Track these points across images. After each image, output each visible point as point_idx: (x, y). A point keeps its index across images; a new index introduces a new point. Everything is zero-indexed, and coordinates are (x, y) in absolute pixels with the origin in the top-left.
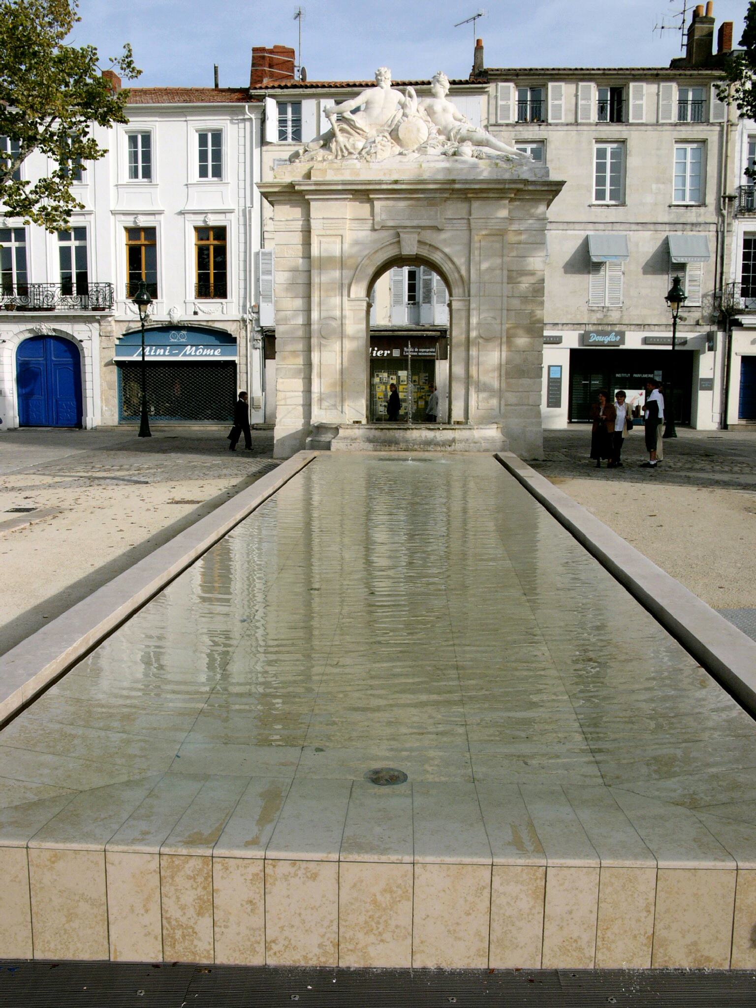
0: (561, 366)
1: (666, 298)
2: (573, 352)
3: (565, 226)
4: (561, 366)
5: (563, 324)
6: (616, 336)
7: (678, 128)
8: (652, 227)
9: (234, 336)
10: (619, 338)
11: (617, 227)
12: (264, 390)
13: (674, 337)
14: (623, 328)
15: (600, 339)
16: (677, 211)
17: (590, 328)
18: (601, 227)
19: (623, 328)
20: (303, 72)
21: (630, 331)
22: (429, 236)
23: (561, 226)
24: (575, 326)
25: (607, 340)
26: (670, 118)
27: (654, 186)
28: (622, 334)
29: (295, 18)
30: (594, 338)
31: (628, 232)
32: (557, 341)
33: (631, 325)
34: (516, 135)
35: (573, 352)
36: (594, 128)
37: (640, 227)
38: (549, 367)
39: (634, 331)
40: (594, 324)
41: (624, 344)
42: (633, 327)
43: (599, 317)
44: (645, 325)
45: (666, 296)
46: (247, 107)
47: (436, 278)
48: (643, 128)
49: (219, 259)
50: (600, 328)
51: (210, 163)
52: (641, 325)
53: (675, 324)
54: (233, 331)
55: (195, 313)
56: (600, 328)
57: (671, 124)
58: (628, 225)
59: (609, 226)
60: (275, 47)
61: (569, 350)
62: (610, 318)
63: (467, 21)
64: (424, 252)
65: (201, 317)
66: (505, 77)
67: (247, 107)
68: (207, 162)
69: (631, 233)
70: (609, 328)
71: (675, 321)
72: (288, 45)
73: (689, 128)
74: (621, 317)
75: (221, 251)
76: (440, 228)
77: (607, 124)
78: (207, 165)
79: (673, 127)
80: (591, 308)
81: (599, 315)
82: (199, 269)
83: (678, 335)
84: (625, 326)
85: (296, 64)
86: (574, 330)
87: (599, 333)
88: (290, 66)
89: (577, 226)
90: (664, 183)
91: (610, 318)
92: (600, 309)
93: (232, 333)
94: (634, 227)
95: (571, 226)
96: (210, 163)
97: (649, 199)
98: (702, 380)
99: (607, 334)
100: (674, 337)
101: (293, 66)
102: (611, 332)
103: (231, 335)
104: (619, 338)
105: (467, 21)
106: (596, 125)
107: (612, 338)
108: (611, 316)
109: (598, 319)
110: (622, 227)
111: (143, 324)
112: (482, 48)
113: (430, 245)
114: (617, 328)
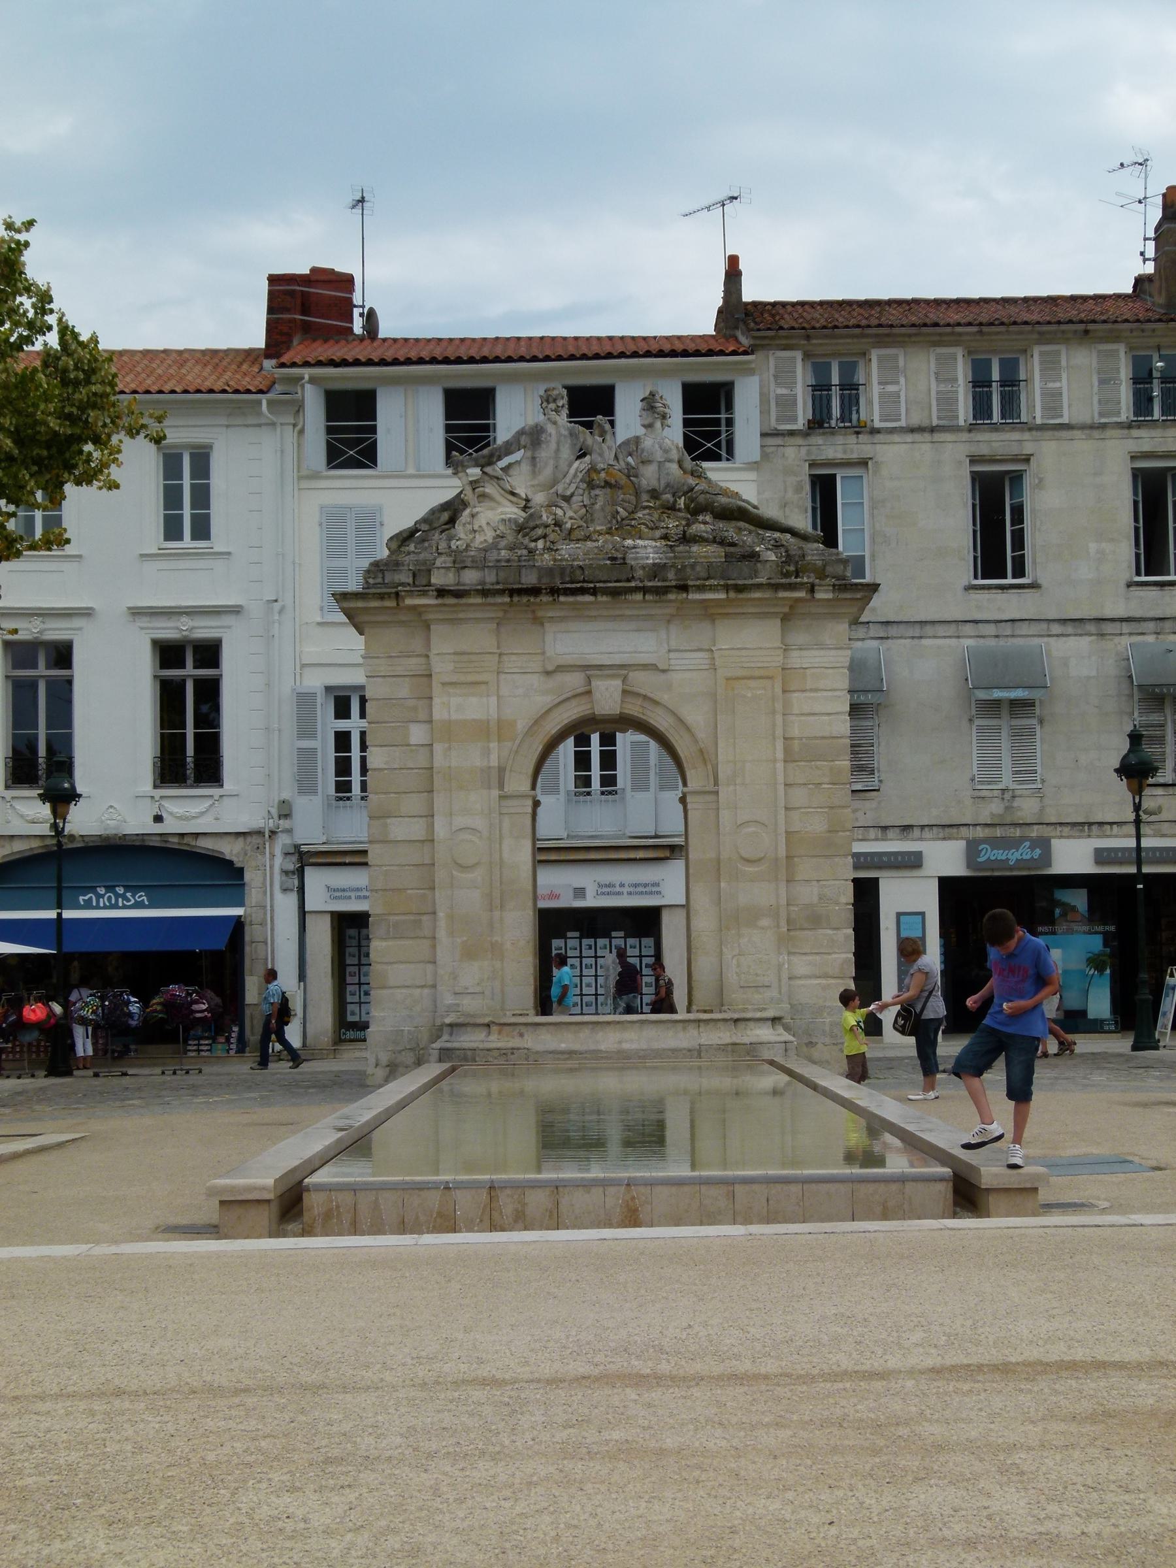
0: (923, 914)
1: (1116, 771)
2: (947, 885)
3: (917, 631)
4: (923, 914)
5: (923, 827)
6: (1032, 848)
7: (1135, 433)
8: (1091, 628)
9: (238, 865)
10: (1038, 851)
11: (1024, 629)
12: (302, 977)
13: (1139, 848)
14: (1046, 831)
15: (1000, 855)
16: (1142, 594)
17: (980, 833)
18: (990, 629)
19: (1046, 831)
20: (371, 317)
21: (1061, 837)
22: (642, 681)
23: (911, 631)
24: (947, 830)
25: (1013, 856)
26: (1119, 414)
27: (1093, 547)
28: (1045, 844)
29: (354, 207)
30: (988, 854)
31: (1046, 639)
32: (912, 862)
33: (1061, 824)
34: (809, 452)
35: (947, 885)
36: (965, 436)
37: (1069, 629)
38: (899, 915)
39: (1068, 837)
40: (986, 825)
41: (1049, 865)
42: (1066, 830)
43: (995, 812)
44: (1090, 824)
45: (1118, 766)
46: (264, 403)
47: (306, 1180)
48: (1064, 434)
49: (205, 708)
50: (999, 832)
51: (187, 512)
52: (1083, 824)
53: (1138, 822)
54: (237, 855)
55: (158, 819)
56: (999, 832)
57: (1120, 425)
58: (1044, 626)
59: (1007, 629)
60: (314, 270)
61: (937, 880)
62: (1019, 813)
63: (708, 208)
64: (634, 709)
65: (170, 826)
66: (784, 342)
67: (264, 403)
68: (192, 515)
69: (1052, 640)
70: (1018, 832)
71: (1138, 816)
72: (341, 268)
73: (1157, 433)
74: (1042, 809)
75: (209, 692)
76: (661, 667)
77: (995, 428)
78: (182, 515)
79: (1126, 431)
80: (977, 794)
81: (995, 808)
82: (162, 727)
83: (1145, 843)
84: (1050, 828)
85: (357, 299)
86: (944, 839)
87: (995, 843)
88: (345, 308)
89: (941, 630)
90: (1112, 540)
91: (1019, 813)
92: (996, 793)
93: (234, 859)
94: (1056, 629)
95: (929, 630)
96: (187, 512)
97: (1085, 572)
98: (970, 863)
99: (1015, 843)
100: (1139, 848)
101: (349, 305)
102: (1023, 839)
103: (231, 863)
104: (1038, 851)
105: (708, 208)
106: (970, 431)
107: (1024, 853)
108: (1019, 808)
109: (992, 815)
110: (1034, 629)
111: (59, 841)
112: (738, 274)
113: (645, 697)
114: (1034, 832)
